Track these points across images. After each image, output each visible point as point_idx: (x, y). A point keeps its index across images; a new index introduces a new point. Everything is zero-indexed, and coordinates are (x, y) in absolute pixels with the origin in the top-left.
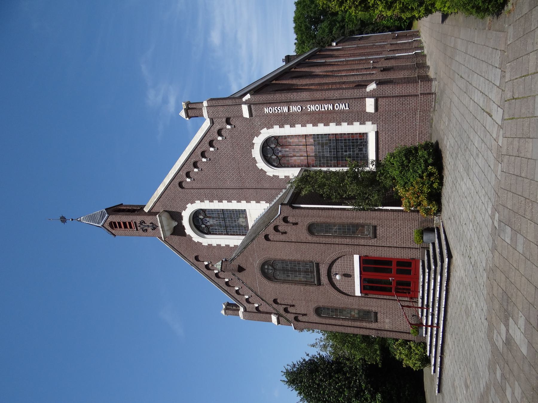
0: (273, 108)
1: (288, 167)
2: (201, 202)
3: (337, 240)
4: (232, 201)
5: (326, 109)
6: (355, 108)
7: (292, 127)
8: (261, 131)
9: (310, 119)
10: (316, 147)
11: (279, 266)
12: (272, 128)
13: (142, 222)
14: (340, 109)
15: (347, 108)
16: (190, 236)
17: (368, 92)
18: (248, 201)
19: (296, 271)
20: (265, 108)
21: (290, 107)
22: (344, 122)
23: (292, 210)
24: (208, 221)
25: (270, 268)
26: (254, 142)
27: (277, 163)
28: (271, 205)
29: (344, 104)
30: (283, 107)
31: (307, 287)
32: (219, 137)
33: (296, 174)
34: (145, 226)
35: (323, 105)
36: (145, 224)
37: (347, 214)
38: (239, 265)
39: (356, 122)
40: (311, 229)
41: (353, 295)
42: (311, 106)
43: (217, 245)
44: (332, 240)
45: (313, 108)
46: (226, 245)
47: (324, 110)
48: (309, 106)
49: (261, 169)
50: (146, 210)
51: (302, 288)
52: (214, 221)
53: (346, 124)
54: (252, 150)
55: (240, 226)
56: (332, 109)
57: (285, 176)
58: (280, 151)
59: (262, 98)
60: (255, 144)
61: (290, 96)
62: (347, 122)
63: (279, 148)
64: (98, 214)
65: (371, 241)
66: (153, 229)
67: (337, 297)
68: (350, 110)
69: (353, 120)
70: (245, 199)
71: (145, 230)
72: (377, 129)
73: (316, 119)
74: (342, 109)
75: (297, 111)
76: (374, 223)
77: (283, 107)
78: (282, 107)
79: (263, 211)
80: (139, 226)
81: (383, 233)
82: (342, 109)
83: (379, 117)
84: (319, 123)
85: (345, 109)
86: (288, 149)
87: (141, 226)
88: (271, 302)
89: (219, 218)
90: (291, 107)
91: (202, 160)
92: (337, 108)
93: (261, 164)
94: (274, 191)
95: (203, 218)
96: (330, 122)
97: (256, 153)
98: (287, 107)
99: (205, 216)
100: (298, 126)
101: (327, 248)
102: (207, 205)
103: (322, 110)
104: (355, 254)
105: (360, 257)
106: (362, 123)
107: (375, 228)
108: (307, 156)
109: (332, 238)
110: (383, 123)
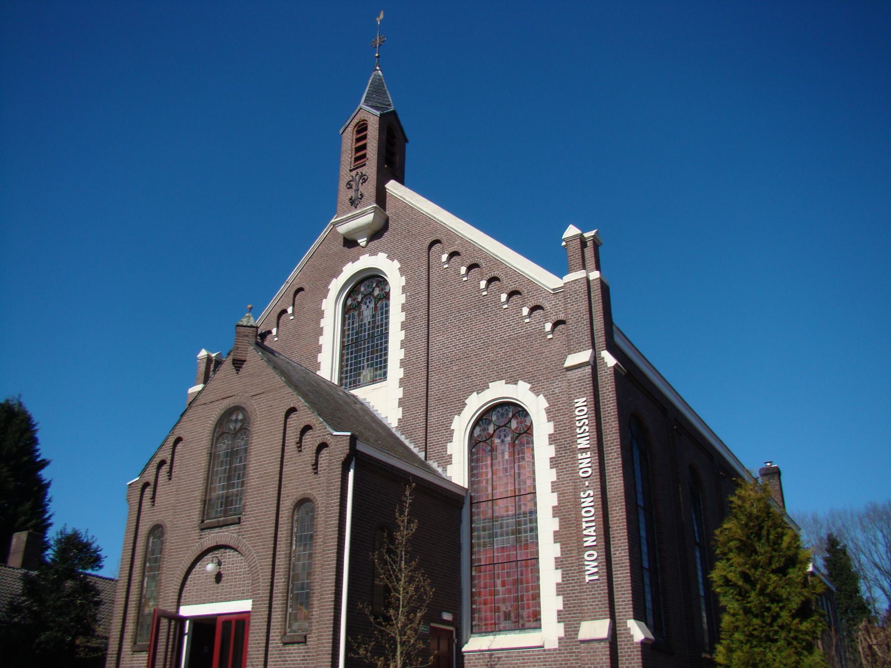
0: (586, 416)
1: (471, 460)
2: (403, 287)
3: (281, 561)
4: (403, 350)
5: (585, 532)
6: (589, 595)
7: (551, 462)
8: (541, 396)
9: (568, 499)
10: (513, 519)
11: (240, 443)
12: (548, 418)
13: (364, 179)
14: (586, 563)
15: (588, 579)
16: (340, 274)
17: (626, 622)
18: (402, 382)
19: (229, 478)
20: (584, 399)
21: (589, 453)
22: (563, 574)
23: (340, 461)
24: (368, 306)
25: (239, 425)
26: (520, 383)
27: (479, 436)
28: (394, 430)
29: (596, 570)
30: (588, 438)
31: (198, 505)
32: (528, 310)
33: (455, 480)
34: (358, 185)
35: (593, 524)
36: (360, 184)
37: (328, 579)
38: (245, 361)
39: (564, 601)
40: (303, 503)
41: (182, 600)
42: (592, 499)
43: (322, 328)
44: (283, 551)
45: (587, 502)
46: (321, 345)
47: (584, 527)
48: (592, 494)
49: (466, 404)
50: (393, 187)
51: (198, 494)
52: (369, 317)
53: (560, 580)
54: (504, 381)
55: (357, 370)
56: (586, 544)
57: (451, 455)
58: (503, 441)
59: (610, 392)
60: (515, 386)
61: (615, 452)
62: (563, 581)
63: (508, 439)
64: (386, 99)
65: (277, 636)
66: (351, 199)
67: (177, 567)
68: (585, 585)
69: (568, 594)
70: (406, 375)
71: (350, 184)
72: (549, 650)
73: (567, 512)
74: (587, 568)
75: (581, 468)
76: (312, 640)
77: (588, 438)
78: (587, 434)
79: (383, 416)
80: (357, 174)
81: (291, 660)
82: (587, 568)
83: (574, 652)
84: (561, 519)
85: (587, 573)
86: (507, 457)
87: (358, 178)
88: (178, 433)
89: (373, 328)
90: (589, 454)
91: (482, 280)
92: (588, 555)
93: (475, 403)
94: (422, 434)
95: (373, 296)
96: (561, 545)
97: (498, 390)
98: (588, 446)
99: (379, 299)
100: (552, 475)
101: (266, 541)
102: (397, 299)
103: (584, 523)
104: (253, 601)
105: (249, 612)
106: (561, 616)
107: (304, 641)
108: (492, 500)
109: (287, 550)
110: (563, 660)
